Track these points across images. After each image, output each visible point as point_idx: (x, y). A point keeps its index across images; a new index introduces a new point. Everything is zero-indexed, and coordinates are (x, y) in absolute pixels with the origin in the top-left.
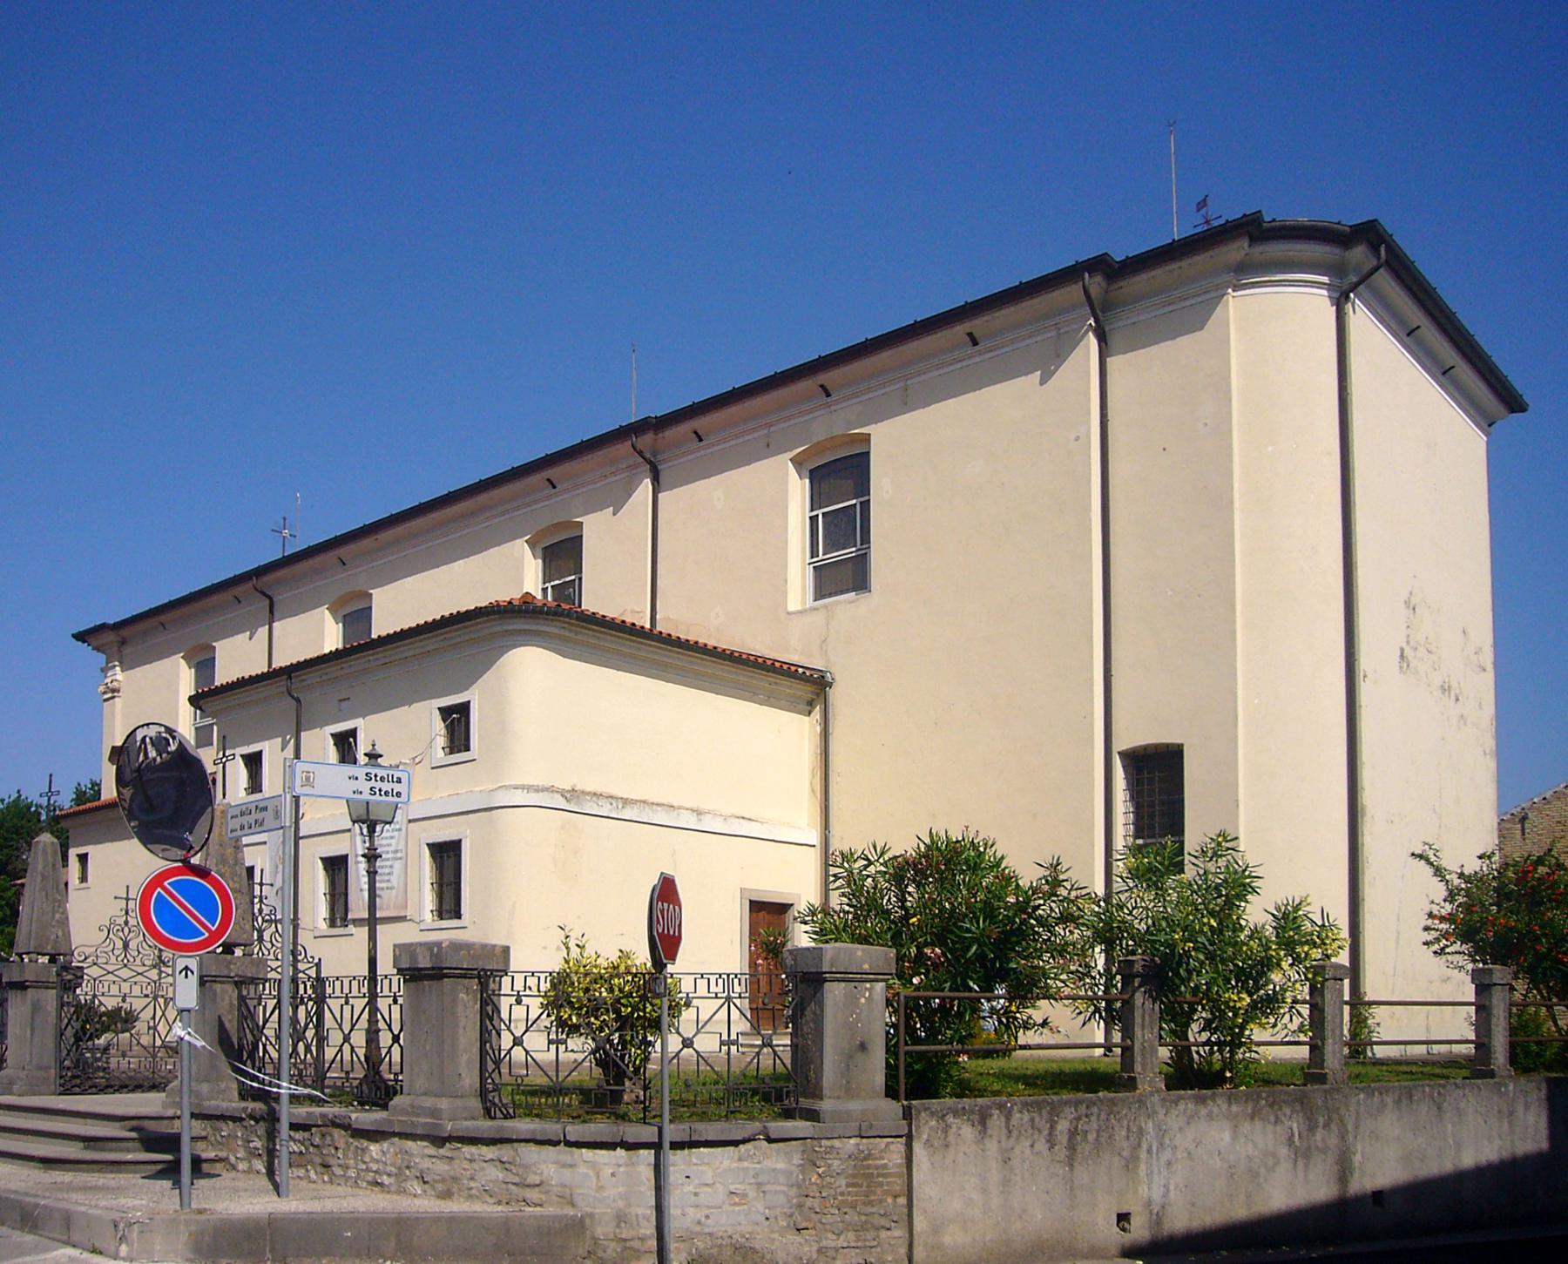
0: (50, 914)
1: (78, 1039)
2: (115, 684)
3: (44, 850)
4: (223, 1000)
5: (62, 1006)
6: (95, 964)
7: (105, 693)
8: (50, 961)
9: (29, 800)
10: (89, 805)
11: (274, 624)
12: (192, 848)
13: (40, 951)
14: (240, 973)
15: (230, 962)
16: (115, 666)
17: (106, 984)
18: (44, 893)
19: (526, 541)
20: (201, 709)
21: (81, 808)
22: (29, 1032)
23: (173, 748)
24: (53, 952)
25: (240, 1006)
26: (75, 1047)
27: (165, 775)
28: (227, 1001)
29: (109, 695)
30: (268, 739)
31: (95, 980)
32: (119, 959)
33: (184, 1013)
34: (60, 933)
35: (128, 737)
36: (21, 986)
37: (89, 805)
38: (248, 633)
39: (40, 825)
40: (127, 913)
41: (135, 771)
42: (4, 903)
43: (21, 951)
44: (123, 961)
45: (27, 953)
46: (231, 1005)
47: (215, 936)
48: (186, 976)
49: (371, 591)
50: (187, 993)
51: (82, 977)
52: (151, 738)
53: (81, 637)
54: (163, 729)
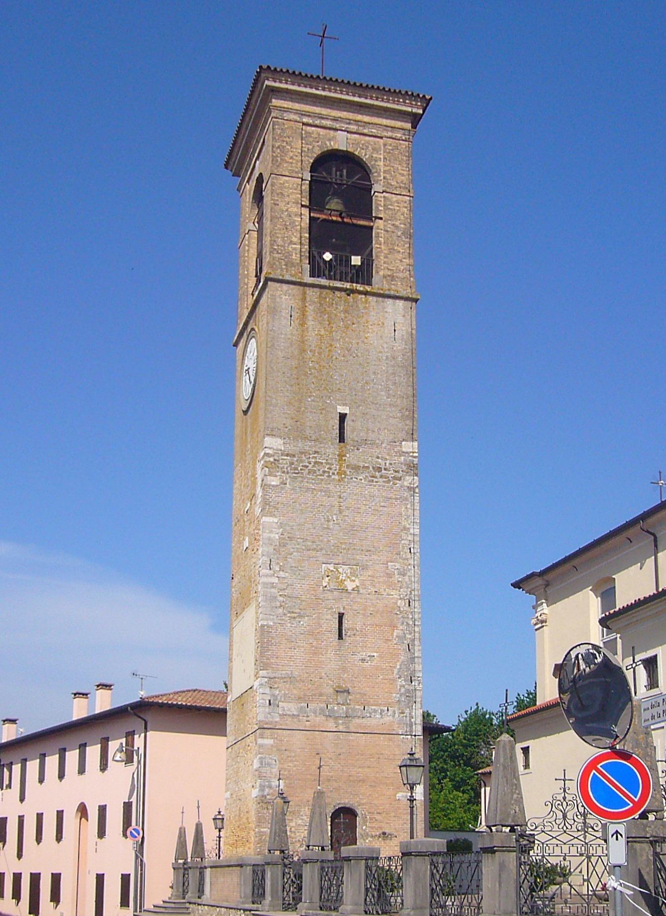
0: (510, 796)
1: (532, 890)
2: (543, 616)
3: (504, 747)
4: (642, 856)
5: (521, 864)
6: (543, 831)
7: (536, 624)
8: (510, 831)
9: (485, 710)
10: (530, 710)
11: (659, 555)
12: (617, 737)
13: (503, 824)
14: (654, 834)
15: (646, 826)
16: (542, 603)
17: (551, 847)
18: (505, 779)
19: (591, 590)
20: (608, 628)
21: (523, 712)
22: (498, 885)
23: (599, 660)
24: (513, 824)
25: (655, 861)
26: (530, 896)
27: (595, 680)
28: (644, 858)
29: (540, 625)
30: (661, 645)
31: (543, 844)
32: (560, 827)
33: (616, 868)
34: (517, 810)
35: (566, 656)
36: (491, 850)
37: (530, 710)
38: (639, 564)
39: (492, 728)
40: (565, 791)
41: (571, 682)
42: (470, 787)
43: (490, 824)
44: (563, 828)
45: (494, 826)
46: (648, 859)
47: (637, 805)
48: (617, 839)
49: (613, 577)
50: (618, 852)
51: (534, 842)
52: (582, 655)
53: (517, 585)
54: (590, 647)
